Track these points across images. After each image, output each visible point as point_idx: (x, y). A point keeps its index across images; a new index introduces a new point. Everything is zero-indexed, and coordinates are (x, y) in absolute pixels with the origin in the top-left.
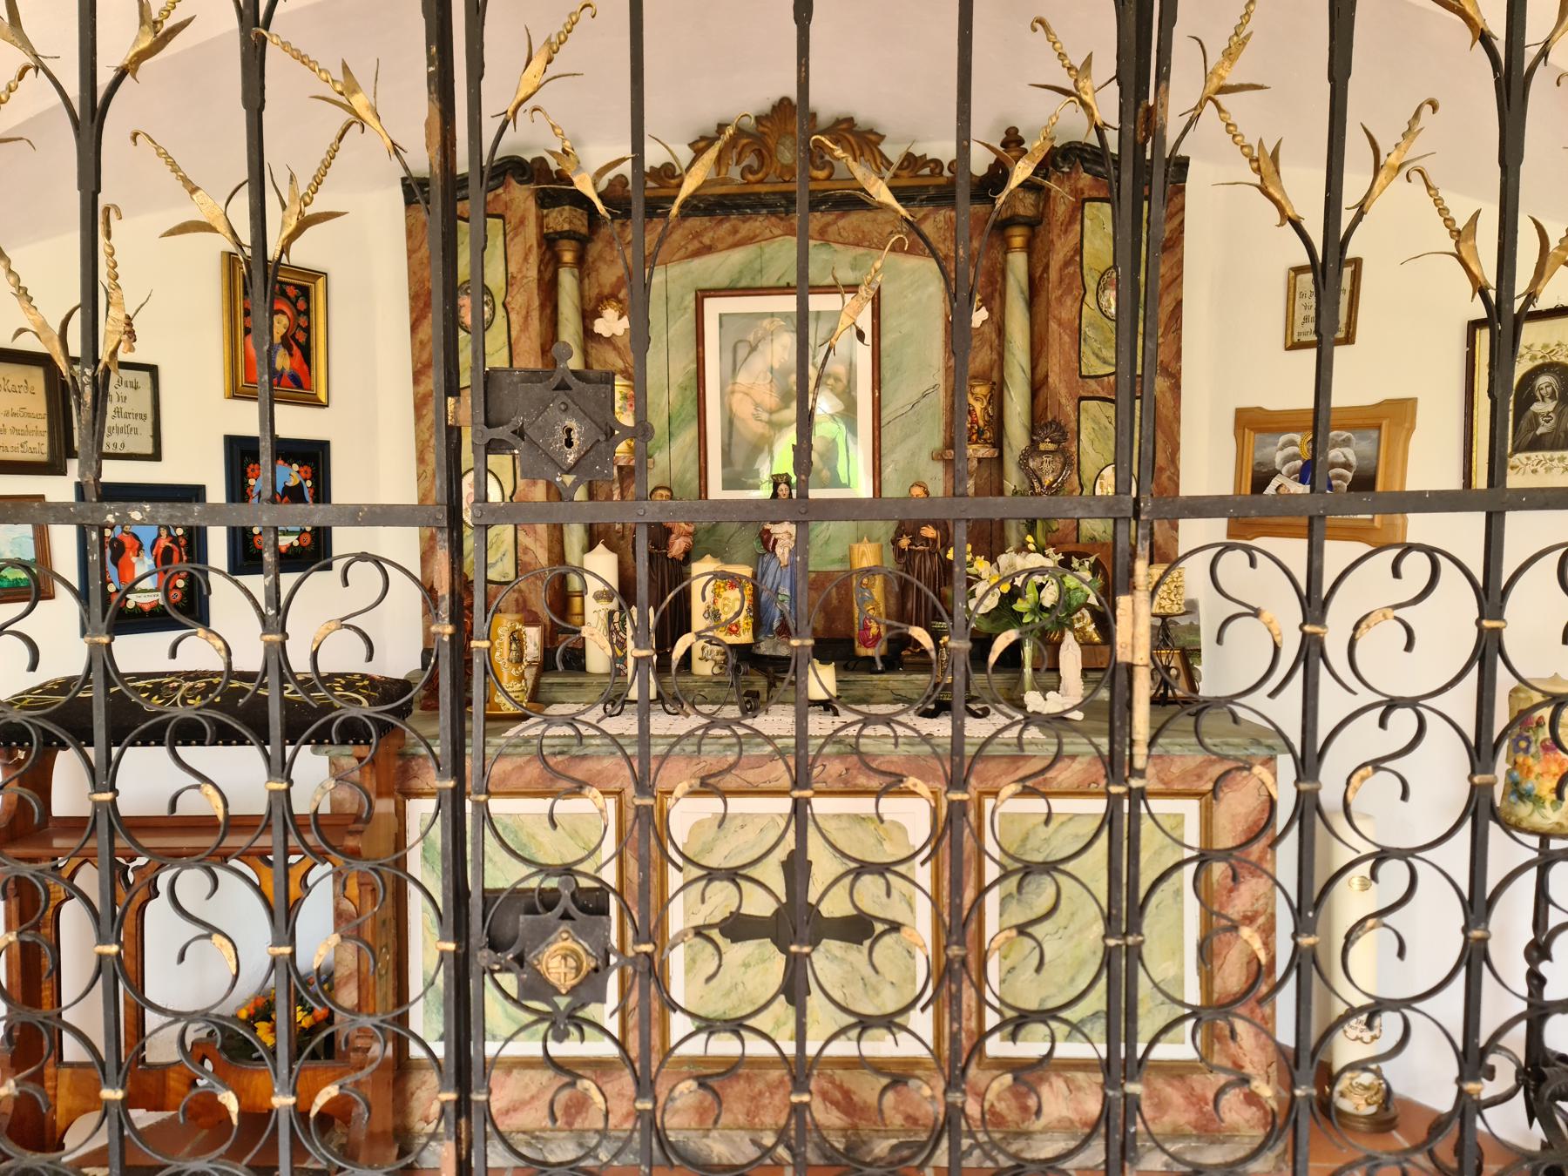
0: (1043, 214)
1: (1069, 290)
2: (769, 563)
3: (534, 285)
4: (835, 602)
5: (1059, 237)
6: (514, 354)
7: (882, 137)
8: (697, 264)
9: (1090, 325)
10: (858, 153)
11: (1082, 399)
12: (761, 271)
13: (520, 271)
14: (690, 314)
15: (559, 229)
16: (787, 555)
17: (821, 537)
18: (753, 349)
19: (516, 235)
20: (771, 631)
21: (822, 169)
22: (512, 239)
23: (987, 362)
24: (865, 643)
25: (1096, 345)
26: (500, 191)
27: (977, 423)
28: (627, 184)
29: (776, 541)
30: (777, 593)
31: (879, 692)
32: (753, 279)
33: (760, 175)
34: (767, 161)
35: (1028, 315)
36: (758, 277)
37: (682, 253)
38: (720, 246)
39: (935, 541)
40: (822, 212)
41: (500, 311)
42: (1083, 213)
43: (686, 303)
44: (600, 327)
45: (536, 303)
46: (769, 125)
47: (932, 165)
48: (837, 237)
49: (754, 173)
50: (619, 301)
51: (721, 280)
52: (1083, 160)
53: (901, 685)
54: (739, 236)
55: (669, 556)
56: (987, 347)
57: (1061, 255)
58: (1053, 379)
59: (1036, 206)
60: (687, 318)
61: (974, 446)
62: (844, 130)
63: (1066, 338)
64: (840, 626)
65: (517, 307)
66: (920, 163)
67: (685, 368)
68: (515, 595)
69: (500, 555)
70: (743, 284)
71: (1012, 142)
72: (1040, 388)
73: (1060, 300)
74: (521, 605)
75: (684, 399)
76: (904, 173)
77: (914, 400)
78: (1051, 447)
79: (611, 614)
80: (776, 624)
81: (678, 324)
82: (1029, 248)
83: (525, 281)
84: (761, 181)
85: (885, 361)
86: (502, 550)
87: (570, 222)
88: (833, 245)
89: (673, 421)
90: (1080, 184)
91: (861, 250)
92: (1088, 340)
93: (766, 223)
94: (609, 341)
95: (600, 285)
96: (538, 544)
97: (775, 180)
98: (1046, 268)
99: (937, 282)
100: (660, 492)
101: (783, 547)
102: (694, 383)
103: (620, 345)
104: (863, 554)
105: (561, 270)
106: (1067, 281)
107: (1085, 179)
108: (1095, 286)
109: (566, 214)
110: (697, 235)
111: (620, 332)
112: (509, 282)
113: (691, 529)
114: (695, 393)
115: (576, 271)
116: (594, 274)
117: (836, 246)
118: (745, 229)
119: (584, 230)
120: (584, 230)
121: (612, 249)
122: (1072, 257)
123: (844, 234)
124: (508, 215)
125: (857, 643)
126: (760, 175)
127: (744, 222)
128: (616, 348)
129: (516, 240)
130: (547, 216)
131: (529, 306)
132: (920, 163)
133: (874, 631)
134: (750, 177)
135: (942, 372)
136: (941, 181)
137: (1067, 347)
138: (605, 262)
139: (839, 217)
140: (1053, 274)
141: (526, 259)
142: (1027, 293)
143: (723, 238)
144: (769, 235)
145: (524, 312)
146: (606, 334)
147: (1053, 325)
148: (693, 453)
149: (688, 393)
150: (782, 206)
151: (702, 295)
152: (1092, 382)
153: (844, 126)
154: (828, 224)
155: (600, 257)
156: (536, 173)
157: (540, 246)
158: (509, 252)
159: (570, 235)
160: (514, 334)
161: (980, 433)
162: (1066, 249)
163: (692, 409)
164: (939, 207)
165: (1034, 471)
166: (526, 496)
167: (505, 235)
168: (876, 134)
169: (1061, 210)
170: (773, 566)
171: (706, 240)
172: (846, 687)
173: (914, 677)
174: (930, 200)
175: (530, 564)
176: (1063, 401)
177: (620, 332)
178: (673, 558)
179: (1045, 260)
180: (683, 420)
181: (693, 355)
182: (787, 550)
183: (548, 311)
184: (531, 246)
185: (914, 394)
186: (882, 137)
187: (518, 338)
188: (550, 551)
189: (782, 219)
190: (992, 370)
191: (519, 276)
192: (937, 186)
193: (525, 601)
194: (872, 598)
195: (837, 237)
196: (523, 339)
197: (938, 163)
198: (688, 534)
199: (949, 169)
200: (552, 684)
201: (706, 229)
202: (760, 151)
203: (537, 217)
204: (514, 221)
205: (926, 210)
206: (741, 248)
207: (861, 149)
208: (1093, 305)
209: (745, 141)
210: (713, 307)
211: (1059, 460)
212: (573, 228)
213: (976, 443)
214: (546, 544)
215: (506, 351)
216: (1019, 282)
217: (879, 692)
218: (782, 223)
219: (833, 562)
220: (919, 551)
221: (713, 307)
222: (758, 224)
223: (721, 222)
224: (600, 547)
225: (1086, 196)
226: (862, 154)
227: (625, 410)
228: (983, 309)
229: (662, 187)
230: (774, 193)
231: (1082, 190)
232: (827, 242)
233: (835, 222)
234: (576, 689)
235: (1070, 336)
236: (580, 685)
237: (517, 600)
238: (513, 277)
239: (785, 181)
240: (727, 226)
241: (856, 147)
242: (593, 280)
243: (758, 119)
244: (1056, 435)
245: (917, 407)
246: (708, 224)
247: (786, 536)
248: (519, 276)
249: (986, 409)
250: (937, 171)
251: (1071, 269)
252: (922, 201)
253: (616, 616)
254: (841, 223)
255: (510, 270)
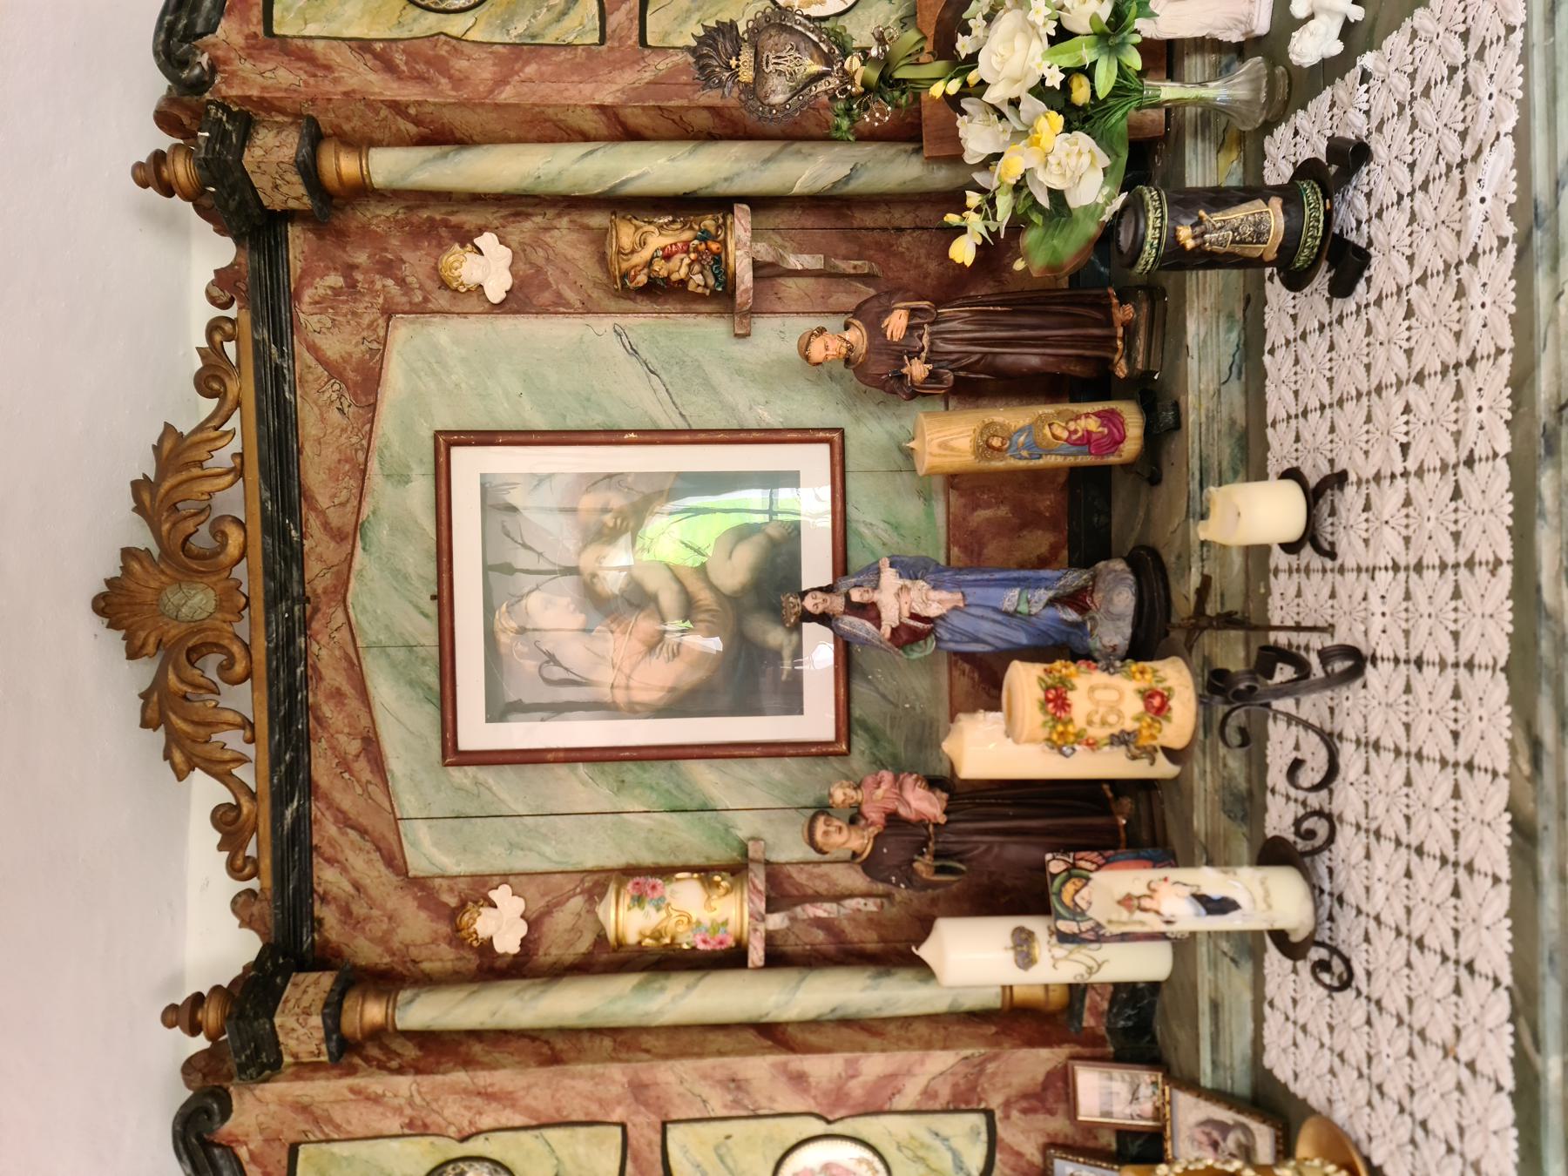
0: (297, 115)
1: (440, 65)
2: (953, 631)
3: (426, 1081)
4: (1003, 511)
5: (336, 81)
6: (558, 1119)
7: (168, 428)
8: (397, 763)
9: (505, 27)
10: (196, 471)
11: (623, 1126)
12: (410, 647)
13: (399, 1111)
14: (486, 774)
15: (321, 1034)
16: (944, 595)
17: (885, 536)
18: (552, 659)
19: (330, 1120)
20: (1079, 626)
21: (224, 535)
22: (338, 1127)
23: (574, 236)
24: (1117, 441)
25: (543, 15)
26: (243, 1153)
27: (687, 243)
28: (250, 893)
29: (914, 616)
30: (1013, 614)
31: (1225, 410)
32: (424, 661)
33: (236, 649)
34: (210, 637)
35: (485, 147)
36: (422, 652)
37: (377, 792)
38: (365, 721)
39: (913, 312)
40: (302, 536)
41: (476, 1147)
42: (294, 37)
43: (467, 782)
44: (508, 942)
45: (460, 1077)
46: (142, 634)
47: (218, 337)
48: (349, 508)
49: (231, 659)
50: (462, 906)
51: (425, 719)
52: (190, 35)
53: (1211, 365)
54: (347, 688)
55: (942, 819)
56: (547, 238)
57: (372, 77)
58: (607, 97)
59: (281, 127)
60: (502, 786)
61: (731, 246)
62: (153, 498)
63: (531, 70)
64: (1046, 502)
65: (468, 1115)
66: (214, 359)
67: (584, 784)
68: (1015, 1114)
69: (937, 1143)
70: (433, 679)
71: (158, 173)
72: (623, 124)
73: (458, 82)
74: (1034, 1103)
75: (640, 784)
76: (233, 388)
77: (642, 370)
78: (747, 55)
79: (1064, 938)
80: (1071, 615)
81: (504, 795)
82: (360, 144)
83: (418, 1100)
84: (247, 648)
85: (572, 423)
86: (928, 1139)
87: (307, 1013)
88: (363, 517)
89: (678, 804)
90: (238, 40)
91: (374, 465)
92: (534, 30)
93: (324, 639)
94: (534, 922)
95: (434, 941)
96: (917, 1069)
97: (246, 620)
98: (397, 107)
99: (431, 329)
100: (819, 837)
101: (926, 601)
102: (609, 767)
103: (542, 903)
104: (944, 445)
105: (400, 1025)
106: (421, 67)
107: (229, 31)
108: (432, 17)
109: (291, 1022)
110: (345, 765)
111: (518, 905)
112: (417, 1128)
113: (887, 776)
114: (629, 765)
115: (404, 996)
116: (414, 952)
117: (366, 510)
118: (333, 675)
119: (327, 980)
120: (327, 980)
121: (367, 919)
122: (376, 56)
123: (344, 495)
124: (290, 1136)
125: (1112, 459)
126: (236, 649)
127: (320, 678)
128: (548, 911)
129: (338, 1118)
130: (295, 1056)
131: (466, 1091)
132: (214, 359)
133: (1093, 425)
134: (240, 668)
135: (591, 319)
136: (246, 319)
137: (547, 69)
138: (391, 931)
139: (313, 507)
140: (409, 93)
141: (376, 1100)
142: (446, 148)
143: (349, 716)
144: (345, 631)
145: (478, 1101)
146: (522, 929)
147: (506, 95)
148: (738, 768)
149: (629, 777)
150: (291, 610)
151: (453, 755)
152: (614, 21)
153: (146, 497)
154: (326, 525)
155: (383, 941)
156: (211, 1082)
157: (352, 1071)
158: (360, 1132)
159: (333, 1010)
160: (519, 1120)
161: (705, 237)
162: (362, 68)
163: (657, 773)
164: (293, 324)
165: (796, 92)
166: (826, 1094)
167: (329, 1141)
168: (161, 440)
169: (282, 77)
170: (957, 621)
171: (354, 746)
172: (1214, 474)
173: (1191, 340)
174: (279, 337)
175: (956, 1085)
176: (648, 76)
177: (518, 905)
178: (946, 812)
179: (384, 112)
180: (678, 786)
181: (562, 770)
182: (934, 595)
183: (477, 1048)
184: (352, 1090)
185: (633, 368)
186: (168, 428)
187: (529, 1111)
188: (928, 1046)
189: (316, 610)
190: (587, 228)
191: (408, 1111)
192: (255, 325)
193: (1025, 1096)
194: (1028, 429)
195: (349, 508)
196: (530, 1101)
197: (213, 327)
198: (898, 783)
199: (226, 306)
200: (1215, 1064)
201: (333, 748)
202: (190, 651)
203: (297, 1077)
204: (302, 1124)
205: (299, 348)
206: (369, 684)
207: (187, 466)
208: (466, 20)
209: (172, 677)
210: (475, 733)
211: (771, 40)
212: (320, 1005)
213: (724, 243)
214: (916, 1055)
215: (552, 1135)
216: (425, 161)
217: (1225, 410)
218: (324, 608)
219: (930, 515)
220: (932, 343)
221: (475, 733)
222: (324, 653)
223: (319, 720)
224: (925, 952)
225: (260, 30)
226: (200, 464)
227: (662, 898)
228: (477, 241)
229: (255, 829)
230: (268, 624)
231: (247, 37)
232: (358, 527)
233: (321, 513)
234: (1225, 1016)
235: (527, 63)
236: (1215, 1007)
237: (1024, 1111)
238: (411, 1125)
239: (247, 604)
240: (327, 710)
241: (184, 475)
242: (425, 953)
243: (133, 654)
244: (724, 45)
245: (654, 364)
246: (324, 744)
247: (904, 597)
248: (408, 1111)
249: (661, 227)
250: (228, 327)
251: (399, 59)
252: (282, 354)
253: (1065, 926)
254: (323, 501)
255: (396, 1129)
